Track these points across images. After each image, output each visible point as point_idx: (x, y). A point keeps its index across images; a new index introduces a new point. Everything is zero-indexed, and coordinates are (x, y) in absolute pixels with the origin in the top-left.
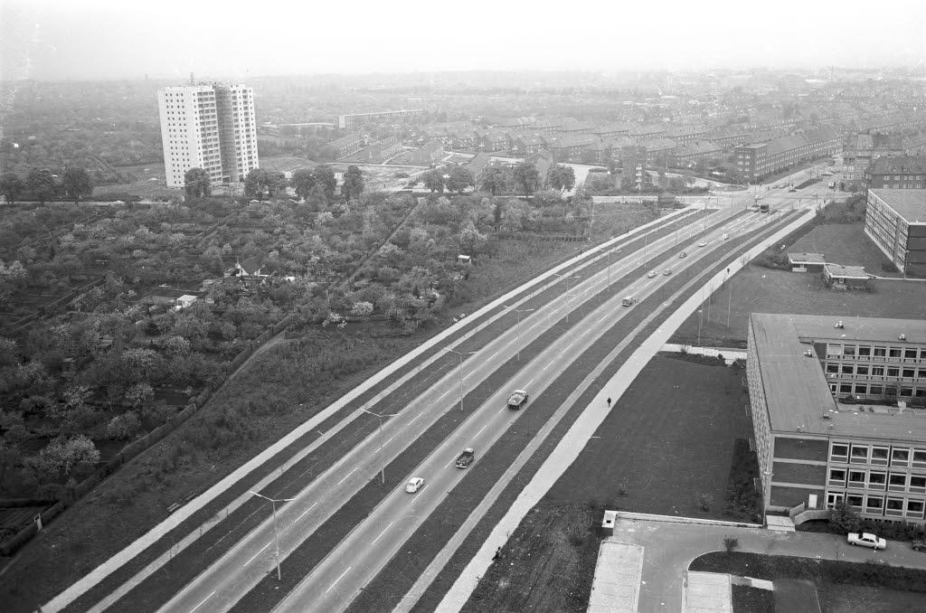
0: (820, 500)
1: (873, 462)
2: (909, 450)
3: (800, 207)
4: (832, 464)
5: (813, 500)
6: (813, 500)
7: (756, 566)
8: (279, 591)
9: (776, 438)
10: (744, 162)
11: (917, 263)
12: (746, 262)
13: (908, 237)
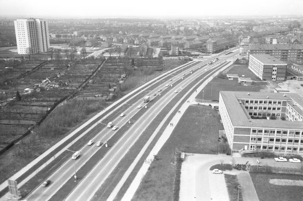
0: (248, 147)
1: (277, 135)
2: (275, 130)
3: (228, 61)
4: (252, 135)
5: (246, 147)
6: (246, 147)
7: (228, 167)
8: (76, 182)
9: (235, 128)
10: (210, 47)
11: (267, 77)
12: (214, 77)
13: (264, 68)
